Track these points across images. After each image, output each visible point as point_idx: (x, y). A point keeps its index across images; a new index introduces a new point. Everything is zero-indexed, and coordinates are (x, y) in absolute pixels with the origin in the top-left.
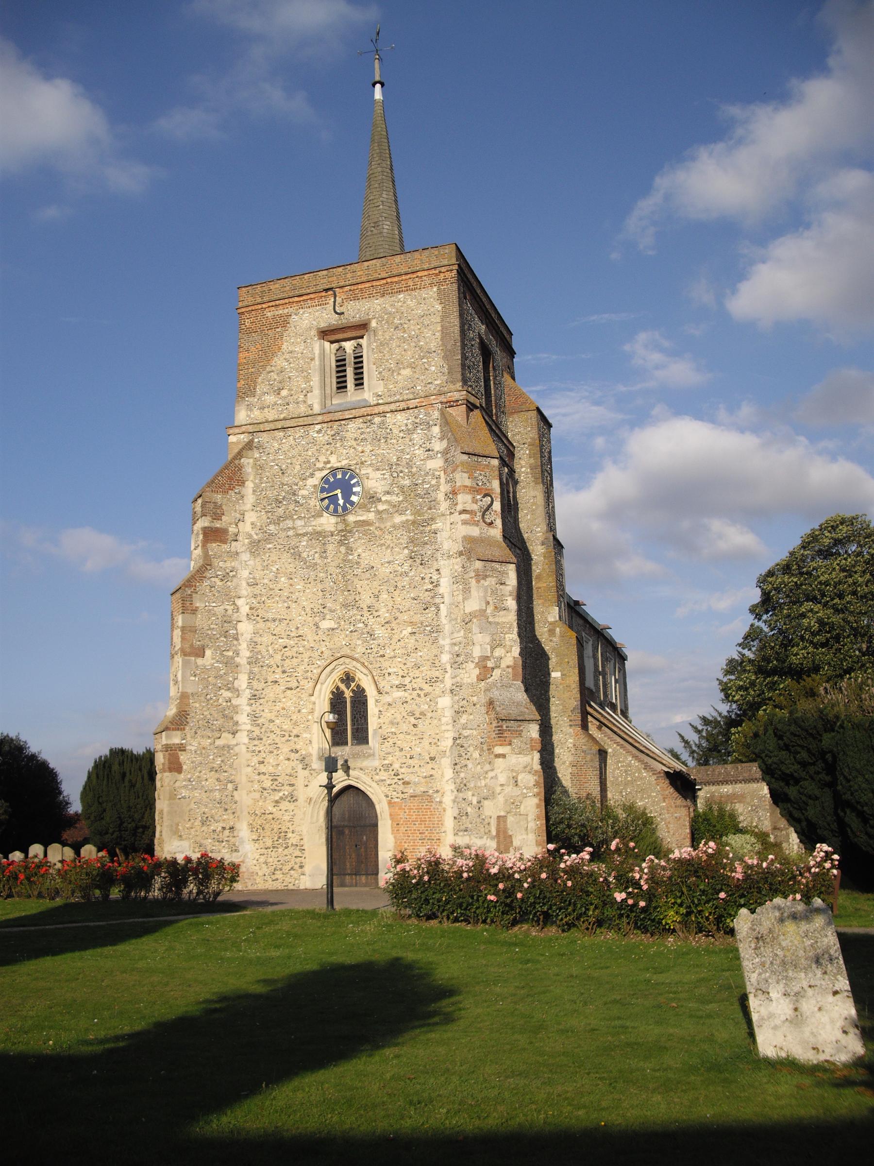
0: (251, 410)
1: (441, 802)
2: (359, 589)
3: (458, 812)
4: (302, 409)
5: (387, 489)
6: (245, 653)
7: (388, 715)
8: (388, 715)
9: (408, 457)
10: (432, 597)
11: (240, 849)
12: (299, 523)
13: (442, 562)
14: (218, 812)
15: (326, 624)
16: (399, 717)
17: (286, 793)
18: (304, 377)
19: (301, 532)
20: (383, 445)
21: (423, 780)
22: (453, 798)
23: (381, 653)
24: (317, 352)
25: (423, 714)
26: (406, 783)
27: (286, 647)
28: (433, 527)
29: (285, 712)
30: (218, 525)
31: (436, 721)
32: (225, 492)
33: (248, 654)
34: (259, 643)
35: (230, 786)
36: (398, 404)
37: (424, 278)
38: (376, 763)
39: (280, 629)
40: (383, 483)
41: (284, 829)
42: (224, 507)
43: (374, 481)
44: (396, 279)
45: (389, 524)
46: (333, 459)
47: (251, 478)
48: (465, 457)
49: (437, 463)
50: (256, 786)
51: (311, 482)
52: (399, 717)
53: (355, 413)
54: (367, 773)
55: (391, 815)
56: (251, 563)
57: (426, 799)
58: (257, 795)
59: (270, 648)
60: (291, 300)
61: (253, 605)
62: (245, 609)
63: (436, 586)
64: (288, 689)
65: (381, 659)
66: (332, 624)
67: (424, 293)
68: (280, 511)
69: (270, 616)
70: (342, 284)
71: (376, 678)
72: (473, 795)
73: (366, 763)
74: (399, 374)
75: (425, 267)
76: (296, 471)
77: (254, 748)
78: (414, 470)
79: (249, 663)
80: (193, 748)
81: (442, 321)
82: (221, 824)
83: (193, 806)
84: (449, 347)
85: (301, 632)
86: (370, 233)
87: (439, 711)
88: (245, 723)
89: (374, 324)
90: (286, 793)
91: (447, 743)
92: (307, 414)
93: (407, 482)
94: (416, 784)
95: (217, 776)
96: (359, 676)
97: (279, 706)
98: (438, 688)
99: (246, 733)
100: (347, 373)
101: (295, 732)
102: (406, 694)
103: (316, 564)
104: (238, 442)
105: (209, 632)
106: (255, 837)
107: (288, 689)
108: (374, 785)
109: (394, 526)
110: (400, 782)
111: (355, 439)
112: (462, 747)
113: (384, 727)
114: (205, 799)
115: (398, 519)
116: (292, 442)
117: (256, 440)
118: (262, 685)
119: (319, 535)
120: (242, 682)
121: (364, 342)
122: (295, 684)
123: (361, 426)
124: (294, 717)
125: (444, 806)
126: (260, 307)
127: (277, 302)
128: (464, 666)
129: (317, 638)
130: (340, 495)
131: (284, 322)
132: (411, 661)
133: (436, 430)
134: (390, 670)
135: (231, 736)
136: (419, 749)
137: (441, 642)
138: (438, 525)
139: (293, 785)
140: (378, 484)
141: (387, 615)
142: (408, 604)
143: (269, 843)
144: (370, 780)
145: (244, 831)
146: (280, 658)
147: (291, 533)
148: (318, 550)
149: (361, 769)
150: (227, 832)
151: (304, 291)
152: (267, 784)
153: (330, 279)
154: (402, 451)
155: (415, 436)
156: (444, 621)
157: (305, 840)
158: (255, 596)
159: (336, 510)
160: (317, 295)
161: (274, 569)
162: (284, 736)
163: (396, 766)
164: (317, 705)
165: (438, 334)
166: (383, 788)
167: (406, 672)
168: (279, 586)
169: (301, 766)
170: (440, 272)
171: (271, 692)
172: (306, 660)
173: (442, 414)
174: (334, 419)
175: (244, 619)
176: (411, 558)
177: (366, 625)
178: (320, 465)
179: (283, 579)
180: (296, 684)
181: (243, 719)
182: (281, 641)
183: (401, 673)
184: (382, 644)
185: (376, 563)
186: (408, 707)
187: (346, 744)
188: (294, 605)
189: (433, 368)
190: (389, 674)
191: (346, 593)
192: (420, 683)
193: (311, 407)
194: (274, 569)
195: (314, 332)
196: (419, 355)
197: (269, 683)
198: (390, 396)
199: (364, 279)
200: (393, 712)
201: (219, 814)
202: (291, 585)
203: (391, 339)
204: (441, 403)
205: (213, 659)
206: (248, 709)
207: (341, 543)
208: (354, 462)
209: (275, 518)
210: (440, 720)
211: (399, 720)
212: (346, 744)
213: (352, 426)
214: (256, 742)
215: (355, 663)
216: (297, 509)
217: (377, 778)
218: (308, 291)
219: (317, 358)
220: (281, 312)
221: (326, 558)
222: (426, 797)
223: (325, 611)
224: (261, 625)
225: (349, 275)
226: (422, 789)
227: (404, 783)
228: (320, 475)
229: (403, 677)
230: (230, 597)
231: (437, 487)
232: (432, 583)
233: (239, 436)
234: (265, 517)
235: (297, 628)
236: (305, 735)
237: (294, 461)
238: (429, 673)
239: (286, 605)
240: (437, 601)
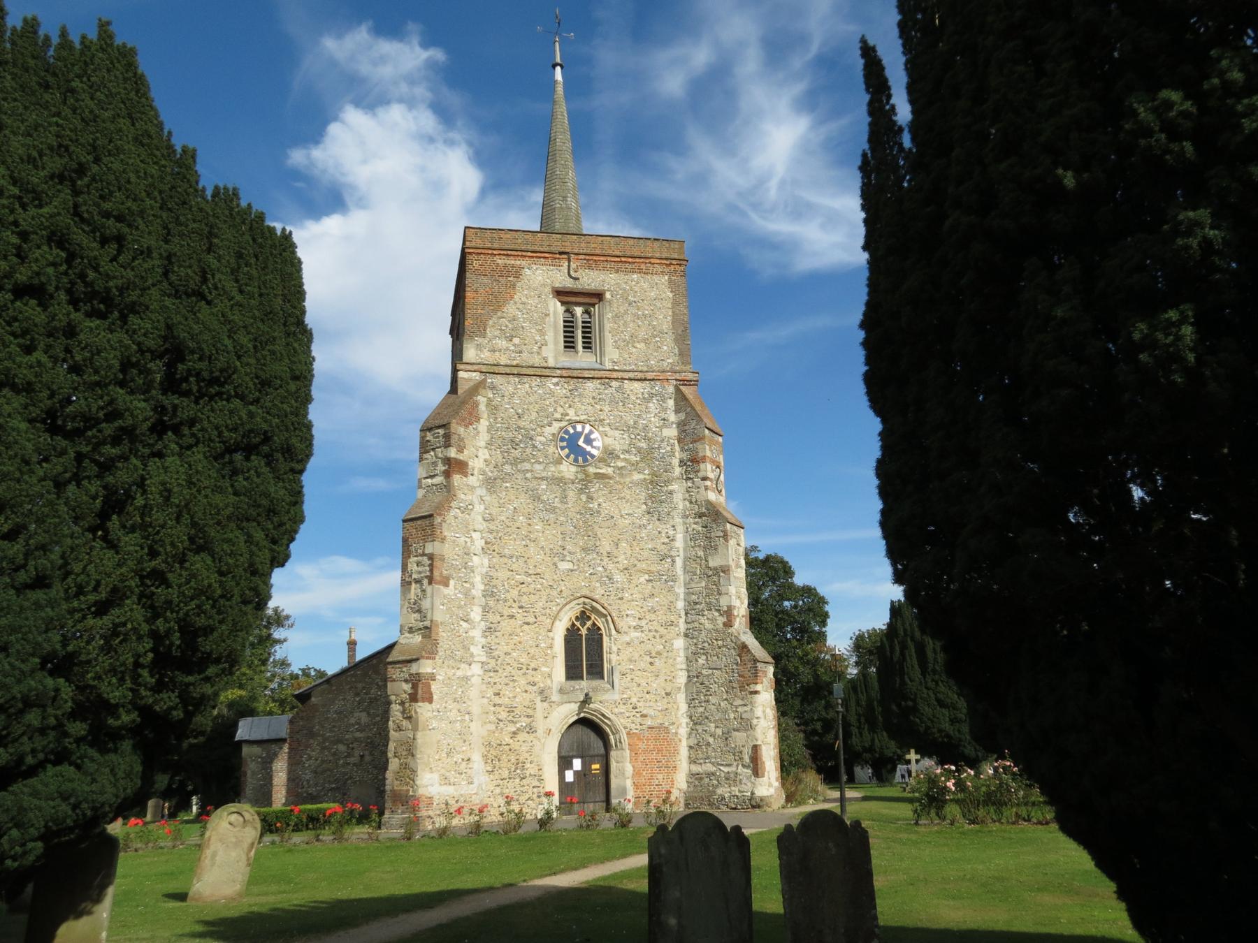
4: (536, 361)
5: (626, 447)
6: (479, 588)
12: (538, 467)
15: (564, 566)
16: (636, 656)
25: (659, 653)
26: (644, 716)
32: (467, 426)
33: (482, 587)
35: (467, 717)
41: (521, 759)
46: (571, 412)
47: (485, 416)
49: (672, 432)
51: (549, 431)
52: (636, 656)
54: (611, 703)
58: (493, 727)
62: (479, 543)
66: (570, 566)
67: (656, 279)
68: (517, 453)
79: (484, 596)
82: (461, 756)
85: (538, 571)
89: (608, 295)
91: (682, 679)
93: (643, 445)
100: (581, 335)
101: (533, 665)
103: (555, 508)
104: (469, 380)
115: (637, 477)
119: (559, 481)
133: (671, 403)
142: (646, 554)
143: (506, 774)
147: (529, 475)
151: (537, 248)
152: (504, 715)
154: (639, 416)
163: (634, 700)
168: (518, 524)
173: (677, 389)
177: (606, 570)
178: (558, 416)
181: (476, 650)
183: (638, 615)
185: (616, 514)
192: (655, 625)
193: (545, 359)
195: (548, 290)
199: (598, 252)
203: (626, 312)
207: (581, 491)
213: (589, 385)
225: (583, 245)
228: (556, 425)
230: (467, 529)
231: (672, 453)
234: (500, 457)
236: (544, 669)
240: (673, 553)
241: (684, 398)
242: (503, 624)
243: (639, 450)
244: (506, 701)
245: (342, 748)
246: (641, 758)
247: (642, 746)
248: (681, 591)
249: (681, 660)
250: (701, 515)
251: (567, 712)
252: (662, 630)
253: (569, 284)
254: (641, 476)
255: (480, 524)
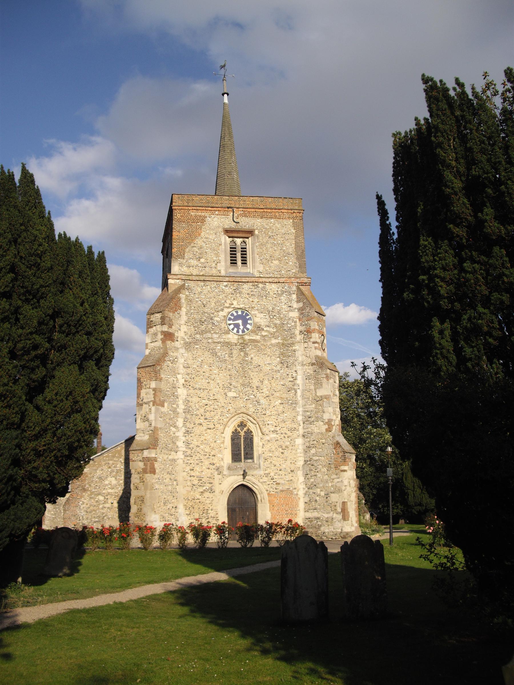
0: (182, 266)
1: (297, 494)
2: (252, 377)
3: (309, 500)
4: (214, 272)
5: (267, 324)
7: (267, 447)
8: (267, 447)
9: (278, 308)
10: (293, 385)
11: (179, 519)
12: (215, 336)
13: (298, 367)
14: (170, 498)
15: (231, 394)
17: (208, 488)
18: (215, 254)
19: (216, 341)
20: (264, 300)
21: (287, 482)
22: (304, 492)
23: (264, 413)
24: (223, 241)
25: (287, 447)
26: (278, 484)
27: (207, 405)
28: (294, 348)
29: (206, 442)
30: (171, 331)
31: (294, 451)
33: (183, 407)
34: (190, 401)
35: (175, 483)
36: (273, 279)
37: (285, 214)
38: (262, 473)
39: (203, 394)
40: (265, 320)
41: (206, 508)
42: (173, 321)
43: (259, 318)
44: (269, 211)
45: (269, 343)
46: (235, 303)
47: (185, 306)
48: (316, 314)
49: (295, 314)
50: (189, 483)
53: (248, 279)
55: (269, 501)
56: (186, 355)
57: (289, 493)
58: (189, 489)
59: (197, 405)
60: (206, 208)
61: (187, 379)
62: (182, 381)
63: (295, 379)
64: (209, 429)
65: (264, 416)
66: (235, 395)
67: (285, 222)
68: (203, 327)
69: (197, 386)
70: (237, 206)
71: (261, 426)
72: (321, 491)
73: (256, 472)
74: (272, 263)
75: (286, 207)
76: (212, 306)
77: (188, 461)
78: (282, 316)
79: (184, 412)
80: (160, 460)
81: (295, 239)
82: (171, 505)
83: (160, 494)
84: (299, 253)
85: (216, 397)
86: (226, 177)
87: (296, 446)
88: (181, 447)
89: (256, 232)
90: (208, 488)
91: (301, 463)
92: (217, 275)
93: (278, 322)
94: (282, 484)
95: (170, 477)
96: (249, 424)
97: (203, 438)
98: (295, 434)
99: (182, 453)
100: (237, 256)
101: (212, 453)
102: (278, 436)
103: (226, 360)
105: (167, 393)
106: (188, 513)
107: (209, 429)
108: (259, 484)
109: (271, 345)
110: (275, 483)
111: (248, 294)
112: (312, 465)
113: (266, 453)
114: (165, 490)
115: (274, 341)
116: (210, 289)
117: (186, 285)
118: (192, 425)
119: (228, 344)
120: (180, 422)
121: (249, 241)
122: (213, 426)
123: (251, 287)
124: (212, 445)
125: (299, 496)
126: (187, 208)
127: (198, 208)
128: (315, 423)
129: (226, 401)
130: (241, 324)
131: (203, 220)
132: (281, 418)
133: (294, 296)
134: (269, 422)
135: (175, 453)
136: (284, 466)
137: (298, 410)
138: (296, 347)
139: (211, 483)
140: (262, 321)
141: (267, 392)
144: (258, 482)
145: (181, 509)
146: (203, 411)
147: (210, 341)
148: (227, 352)
149: (253, 475)
150: (174, 509)
151: (214, 205)
152: (196, 482)
153: (230, 202)
154: (275, 305)
155: (282, 298)
156: (299, 399)
157: (219, 514)
158: (188, 374)
159: (238, 332)
160: (223, 209)
161: (200, 360)
162: (206, 455)
163: (272, 474)
164: (226, 439)
165: (293, 245)
166: (265, 486)
167: (278, 424)
168: (203, 370)
169: (216, 473)
170: (294, 212)
171: (198, 430)
172: (220, 413)
173: (298, 288)
174: (236, 281)
175: (181, 386)
176: (282, 363)
178: (227, 305)
179: (205, 366)
180: (213, 426)
181: (180, 444)
182: (204, 401)
184: (264, 408)
186: (279, 443)
187: (241, 461)
188: (212, 382)
189: (291, 263)
190: (268, 424)
191: (244, 378)
192: (285, 430)
193: (219, 271)
194: (200, 360)
195: (221, 230)
196: (283, 255)
197: (196, 425)
198: (267, 274)
199: (250, 206)
200: (270, 445)
201: (171, 499)
202: (211, 370)
203: (267, 242)
204: (297, 283)
205: (168, 408)
206: (184, 439)
207: (241, 350)
208: (248, 306)
209: (200, 331)
210: (296, 450)
211: (273, 449)
212: (241, 461)
213: (245, 286)
214: (189, 458)
215: (249, 417)
216: (213, 327)
217: (261, 480)
218: (217, 206)
219: (223, 245)
220: (200, 214)
221: (232, 357)
222: (289, 492)
223: (231, 387)
224: (192, 391)
226: (287, 487)
227: (276, 484)
228: (226, 310)
229: (276, 426)
230: (175, 373)
232: (293, 378)
233: (176, 280)
234: (193, 329)
235: (214, 395)
236: (219, 455)
237: (211, 300)
238: (290, 425)
239: (207, 381)
240: (295, 387)
241: (302, 293)
242: (195, 429)
243: (275, 325)
244: (198, 474)
245: (101, 498)
246: (276, 508)
247: (276, 501)
248: (300, 410)
249: (300, 449)
250: (313, 364)
251: (236, 480)
252: (289, 433)
253: (233, 225)
254: (277, 341)
255: (182, 370)
